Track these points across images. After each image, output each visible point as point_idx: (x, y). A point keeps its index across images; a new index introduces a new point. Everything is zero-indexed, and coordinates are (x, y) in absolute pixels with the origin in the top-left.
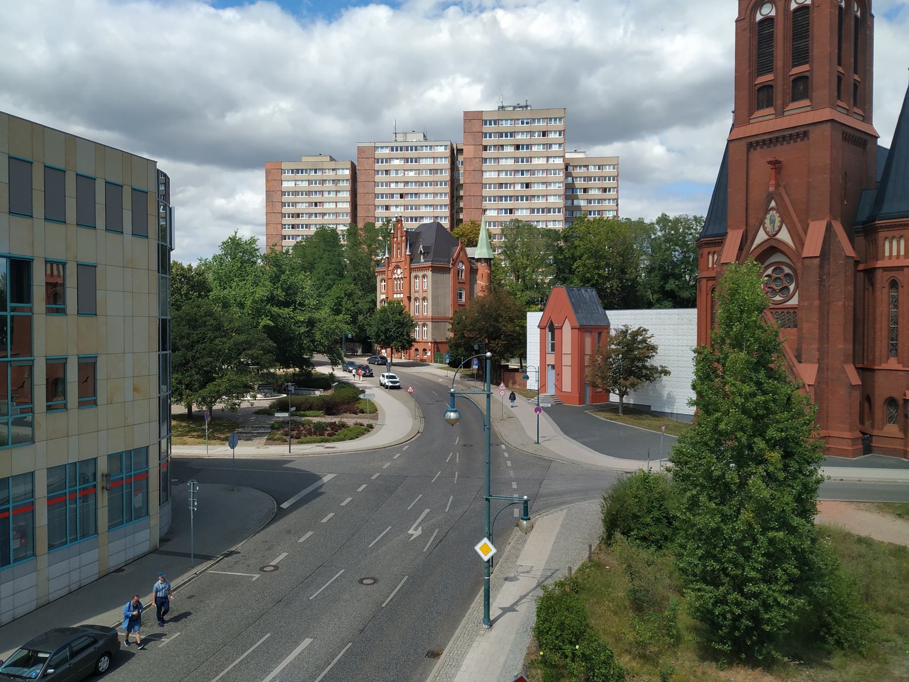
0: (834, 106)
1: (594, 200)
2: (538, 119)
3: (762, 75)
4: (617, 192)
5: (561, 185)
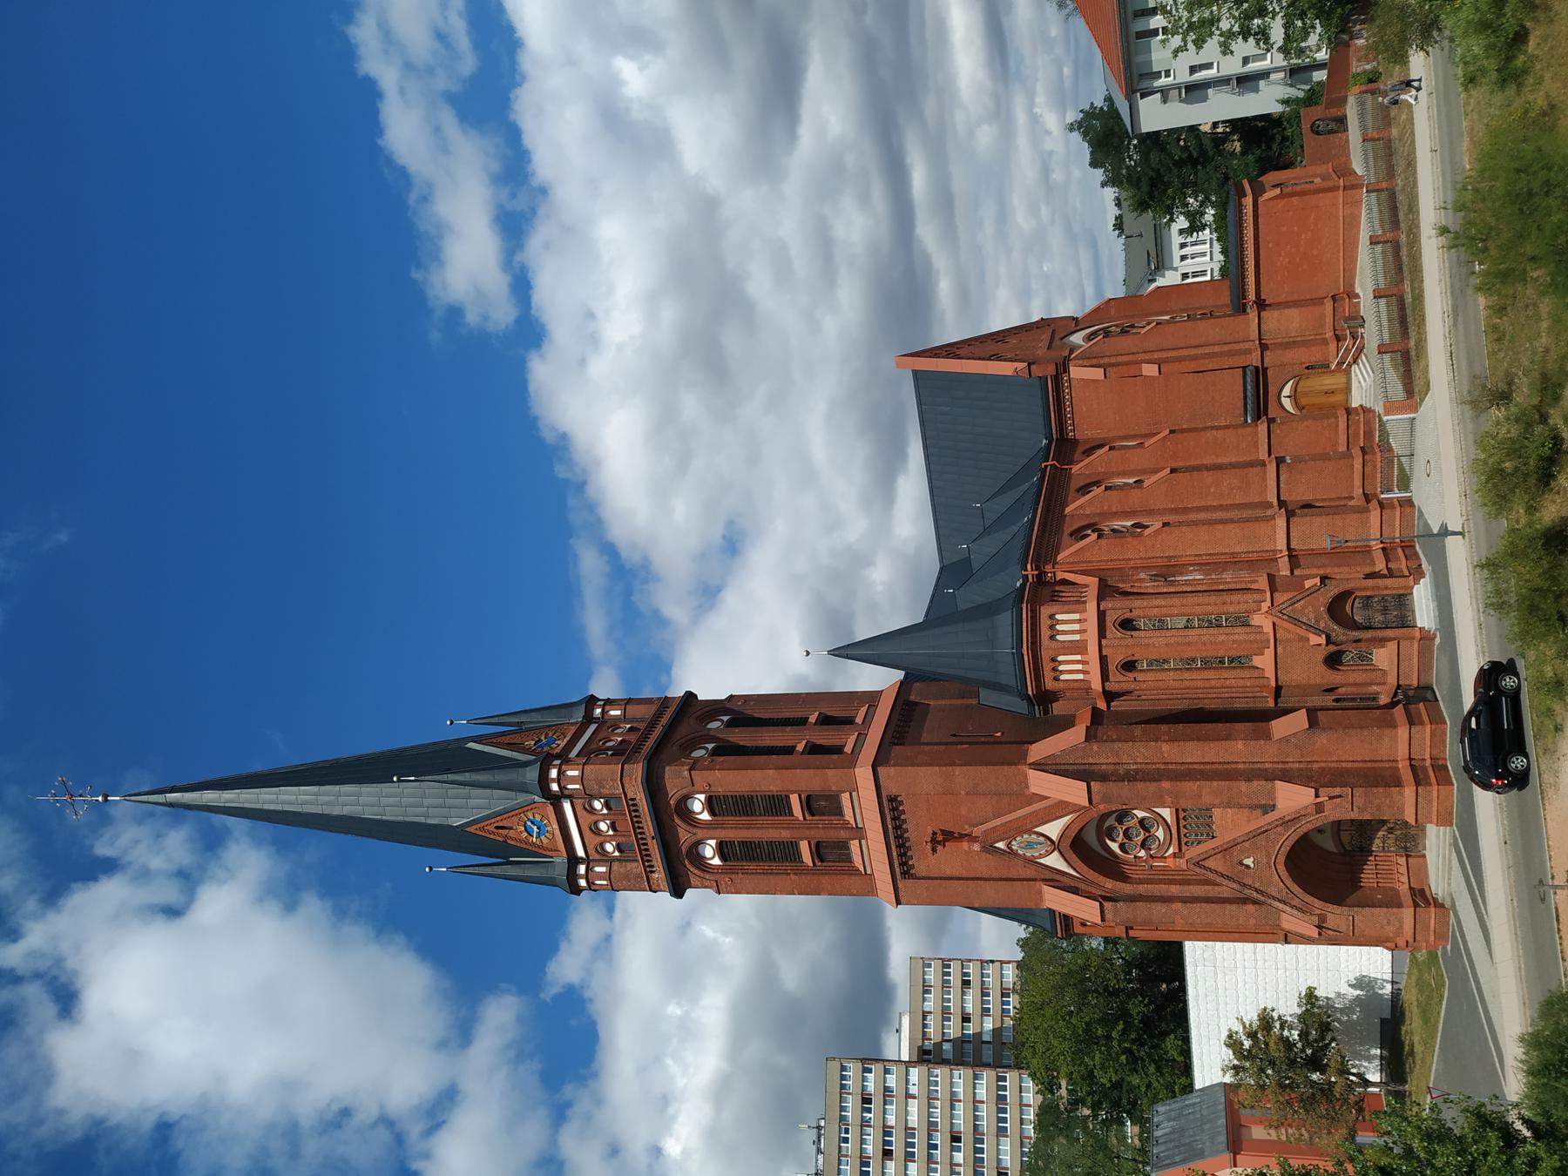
0: (852, 761)
1: (983, 1002)
2: (841, 1111)
3: (800, 855)
4: (970, 961)
5: (956, 1073)
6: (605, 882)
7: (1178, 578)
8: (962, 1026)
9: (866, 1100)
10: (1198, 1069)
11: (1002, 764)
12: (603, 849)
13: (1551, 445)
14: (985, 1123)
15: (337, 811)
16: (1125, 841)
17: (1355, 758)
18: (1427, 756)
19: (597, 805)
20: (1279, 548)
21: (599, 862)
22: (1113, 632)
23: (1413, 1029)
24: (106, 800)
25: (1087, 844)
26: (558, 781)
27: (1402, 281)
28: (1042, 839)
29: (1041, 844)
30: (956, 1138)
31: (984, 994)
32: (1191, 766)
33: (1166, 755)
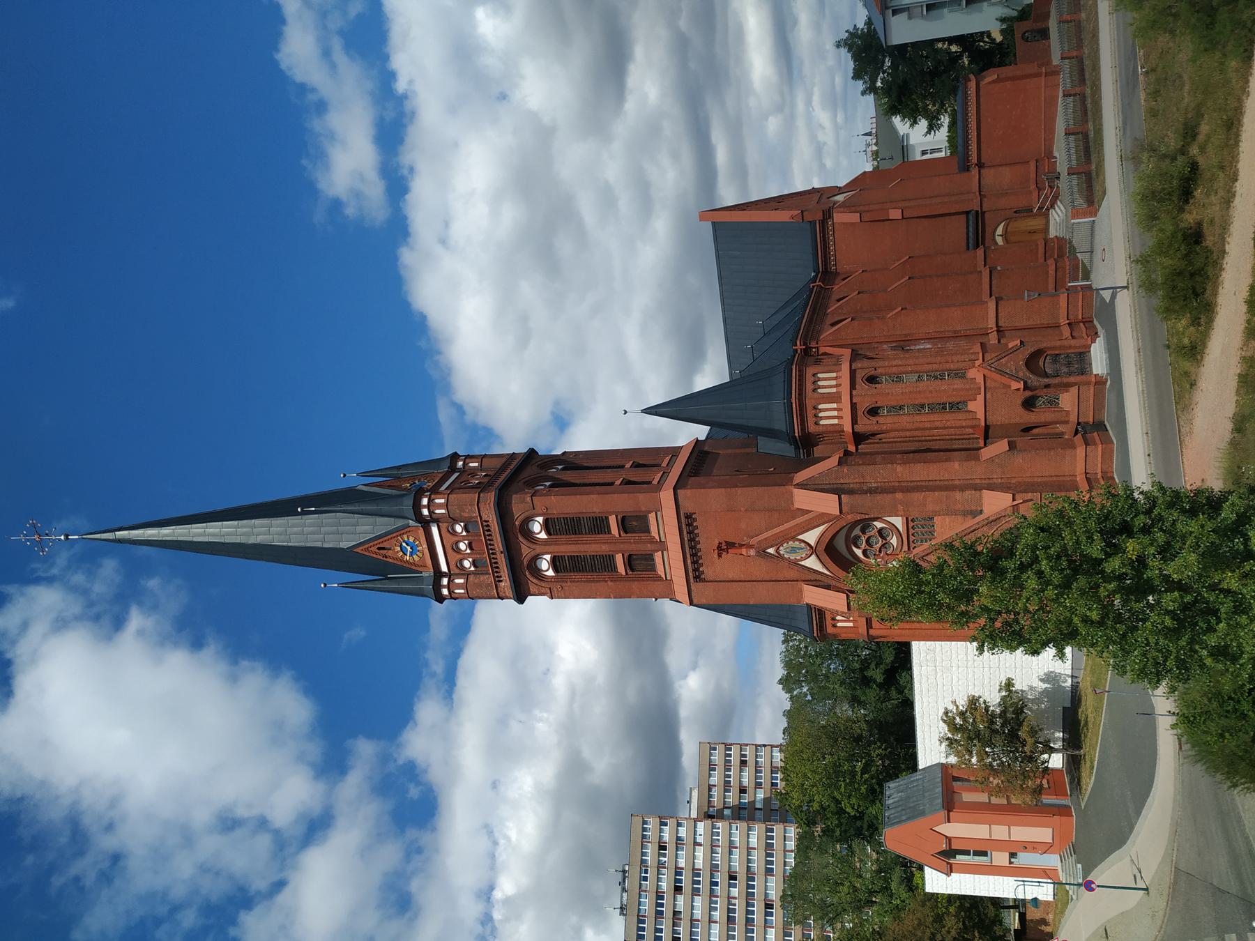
1: (756, 778)
2: (642, 856)
3: (616, 567)
4: (747, 745)
6: (462, 591)
7: (912, 348)
8: (740, 796)
9: (662, 847)
10: (916, 663)
11: (774, 485)
12: (462, 565)
13: (1189, 169)
14: (756, 865)
15: (252, 540)
16: (867, 547)
17: (1044, 474)
18: (1099, 471)
19: (458, 528)
20: (990, 326)
21: (459, 576)
22: (862, 386)
23: (1088, 708)
24: (67, 538)
25: (840, 554)
26: (428, 506)
27: (1087, 122)
28: (803, 545)
29: (802, 549)
30: (732, 877)
31: (758, 770)
32: (918, 484)
33: (900, 475)
